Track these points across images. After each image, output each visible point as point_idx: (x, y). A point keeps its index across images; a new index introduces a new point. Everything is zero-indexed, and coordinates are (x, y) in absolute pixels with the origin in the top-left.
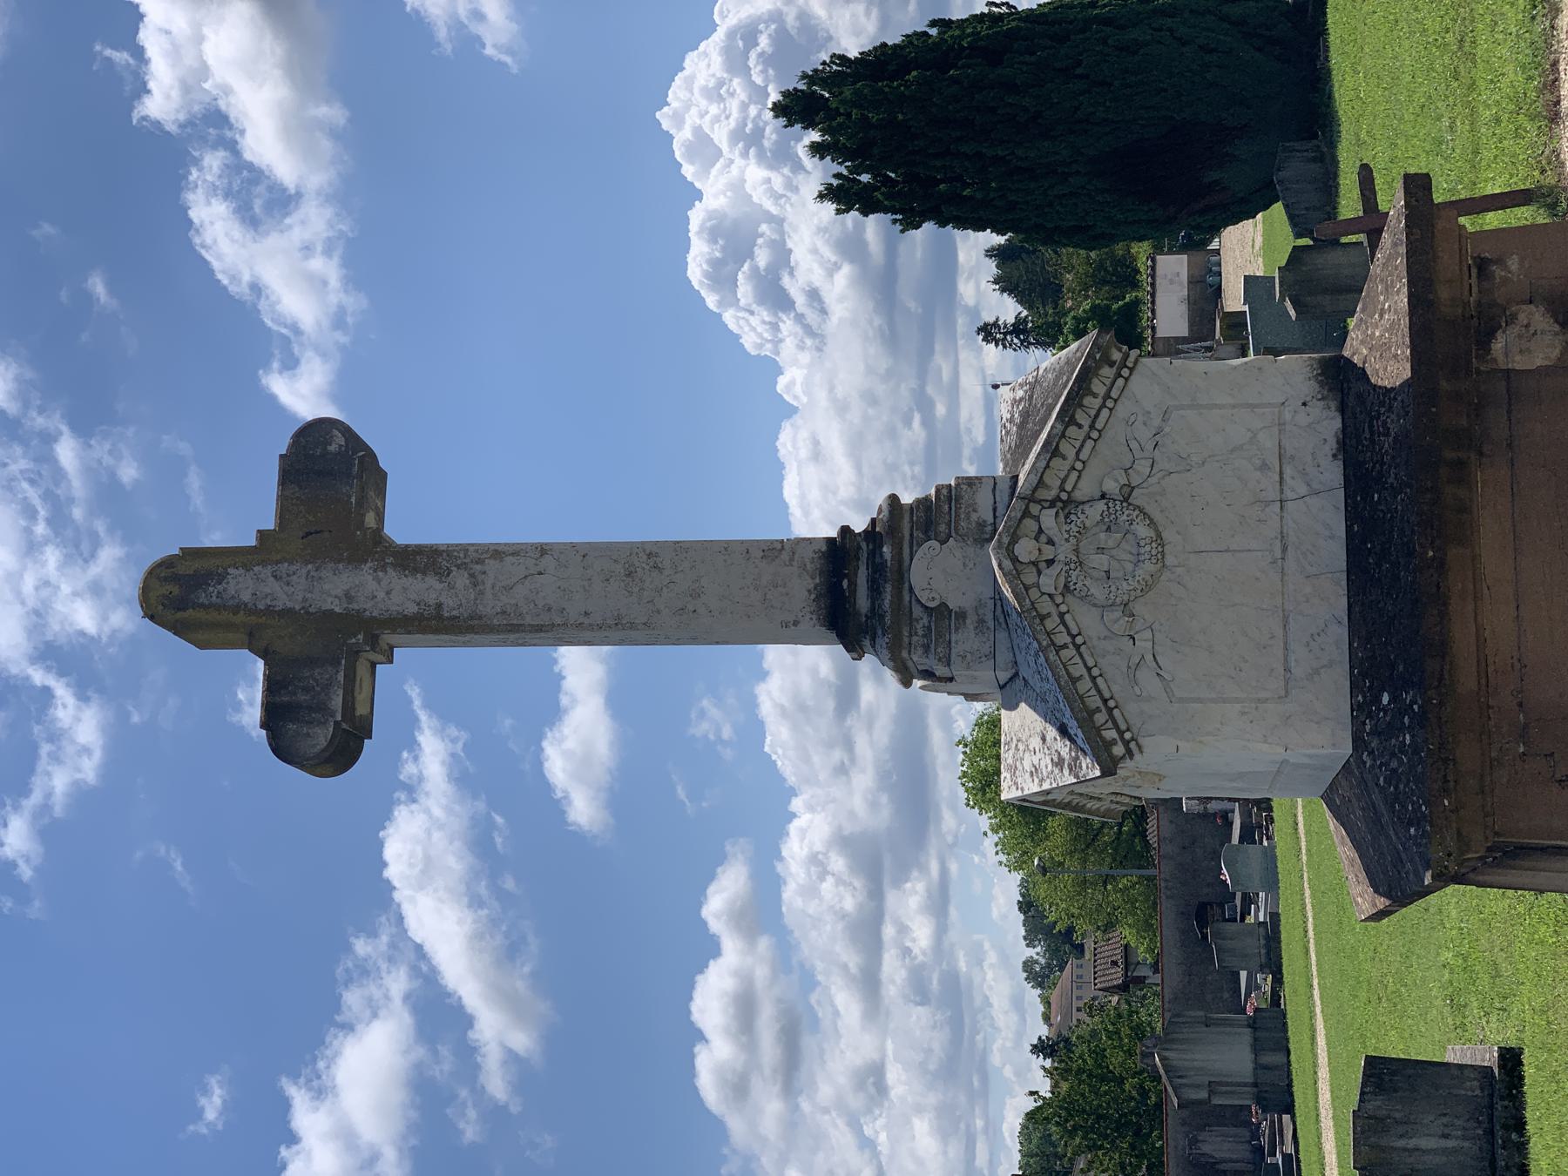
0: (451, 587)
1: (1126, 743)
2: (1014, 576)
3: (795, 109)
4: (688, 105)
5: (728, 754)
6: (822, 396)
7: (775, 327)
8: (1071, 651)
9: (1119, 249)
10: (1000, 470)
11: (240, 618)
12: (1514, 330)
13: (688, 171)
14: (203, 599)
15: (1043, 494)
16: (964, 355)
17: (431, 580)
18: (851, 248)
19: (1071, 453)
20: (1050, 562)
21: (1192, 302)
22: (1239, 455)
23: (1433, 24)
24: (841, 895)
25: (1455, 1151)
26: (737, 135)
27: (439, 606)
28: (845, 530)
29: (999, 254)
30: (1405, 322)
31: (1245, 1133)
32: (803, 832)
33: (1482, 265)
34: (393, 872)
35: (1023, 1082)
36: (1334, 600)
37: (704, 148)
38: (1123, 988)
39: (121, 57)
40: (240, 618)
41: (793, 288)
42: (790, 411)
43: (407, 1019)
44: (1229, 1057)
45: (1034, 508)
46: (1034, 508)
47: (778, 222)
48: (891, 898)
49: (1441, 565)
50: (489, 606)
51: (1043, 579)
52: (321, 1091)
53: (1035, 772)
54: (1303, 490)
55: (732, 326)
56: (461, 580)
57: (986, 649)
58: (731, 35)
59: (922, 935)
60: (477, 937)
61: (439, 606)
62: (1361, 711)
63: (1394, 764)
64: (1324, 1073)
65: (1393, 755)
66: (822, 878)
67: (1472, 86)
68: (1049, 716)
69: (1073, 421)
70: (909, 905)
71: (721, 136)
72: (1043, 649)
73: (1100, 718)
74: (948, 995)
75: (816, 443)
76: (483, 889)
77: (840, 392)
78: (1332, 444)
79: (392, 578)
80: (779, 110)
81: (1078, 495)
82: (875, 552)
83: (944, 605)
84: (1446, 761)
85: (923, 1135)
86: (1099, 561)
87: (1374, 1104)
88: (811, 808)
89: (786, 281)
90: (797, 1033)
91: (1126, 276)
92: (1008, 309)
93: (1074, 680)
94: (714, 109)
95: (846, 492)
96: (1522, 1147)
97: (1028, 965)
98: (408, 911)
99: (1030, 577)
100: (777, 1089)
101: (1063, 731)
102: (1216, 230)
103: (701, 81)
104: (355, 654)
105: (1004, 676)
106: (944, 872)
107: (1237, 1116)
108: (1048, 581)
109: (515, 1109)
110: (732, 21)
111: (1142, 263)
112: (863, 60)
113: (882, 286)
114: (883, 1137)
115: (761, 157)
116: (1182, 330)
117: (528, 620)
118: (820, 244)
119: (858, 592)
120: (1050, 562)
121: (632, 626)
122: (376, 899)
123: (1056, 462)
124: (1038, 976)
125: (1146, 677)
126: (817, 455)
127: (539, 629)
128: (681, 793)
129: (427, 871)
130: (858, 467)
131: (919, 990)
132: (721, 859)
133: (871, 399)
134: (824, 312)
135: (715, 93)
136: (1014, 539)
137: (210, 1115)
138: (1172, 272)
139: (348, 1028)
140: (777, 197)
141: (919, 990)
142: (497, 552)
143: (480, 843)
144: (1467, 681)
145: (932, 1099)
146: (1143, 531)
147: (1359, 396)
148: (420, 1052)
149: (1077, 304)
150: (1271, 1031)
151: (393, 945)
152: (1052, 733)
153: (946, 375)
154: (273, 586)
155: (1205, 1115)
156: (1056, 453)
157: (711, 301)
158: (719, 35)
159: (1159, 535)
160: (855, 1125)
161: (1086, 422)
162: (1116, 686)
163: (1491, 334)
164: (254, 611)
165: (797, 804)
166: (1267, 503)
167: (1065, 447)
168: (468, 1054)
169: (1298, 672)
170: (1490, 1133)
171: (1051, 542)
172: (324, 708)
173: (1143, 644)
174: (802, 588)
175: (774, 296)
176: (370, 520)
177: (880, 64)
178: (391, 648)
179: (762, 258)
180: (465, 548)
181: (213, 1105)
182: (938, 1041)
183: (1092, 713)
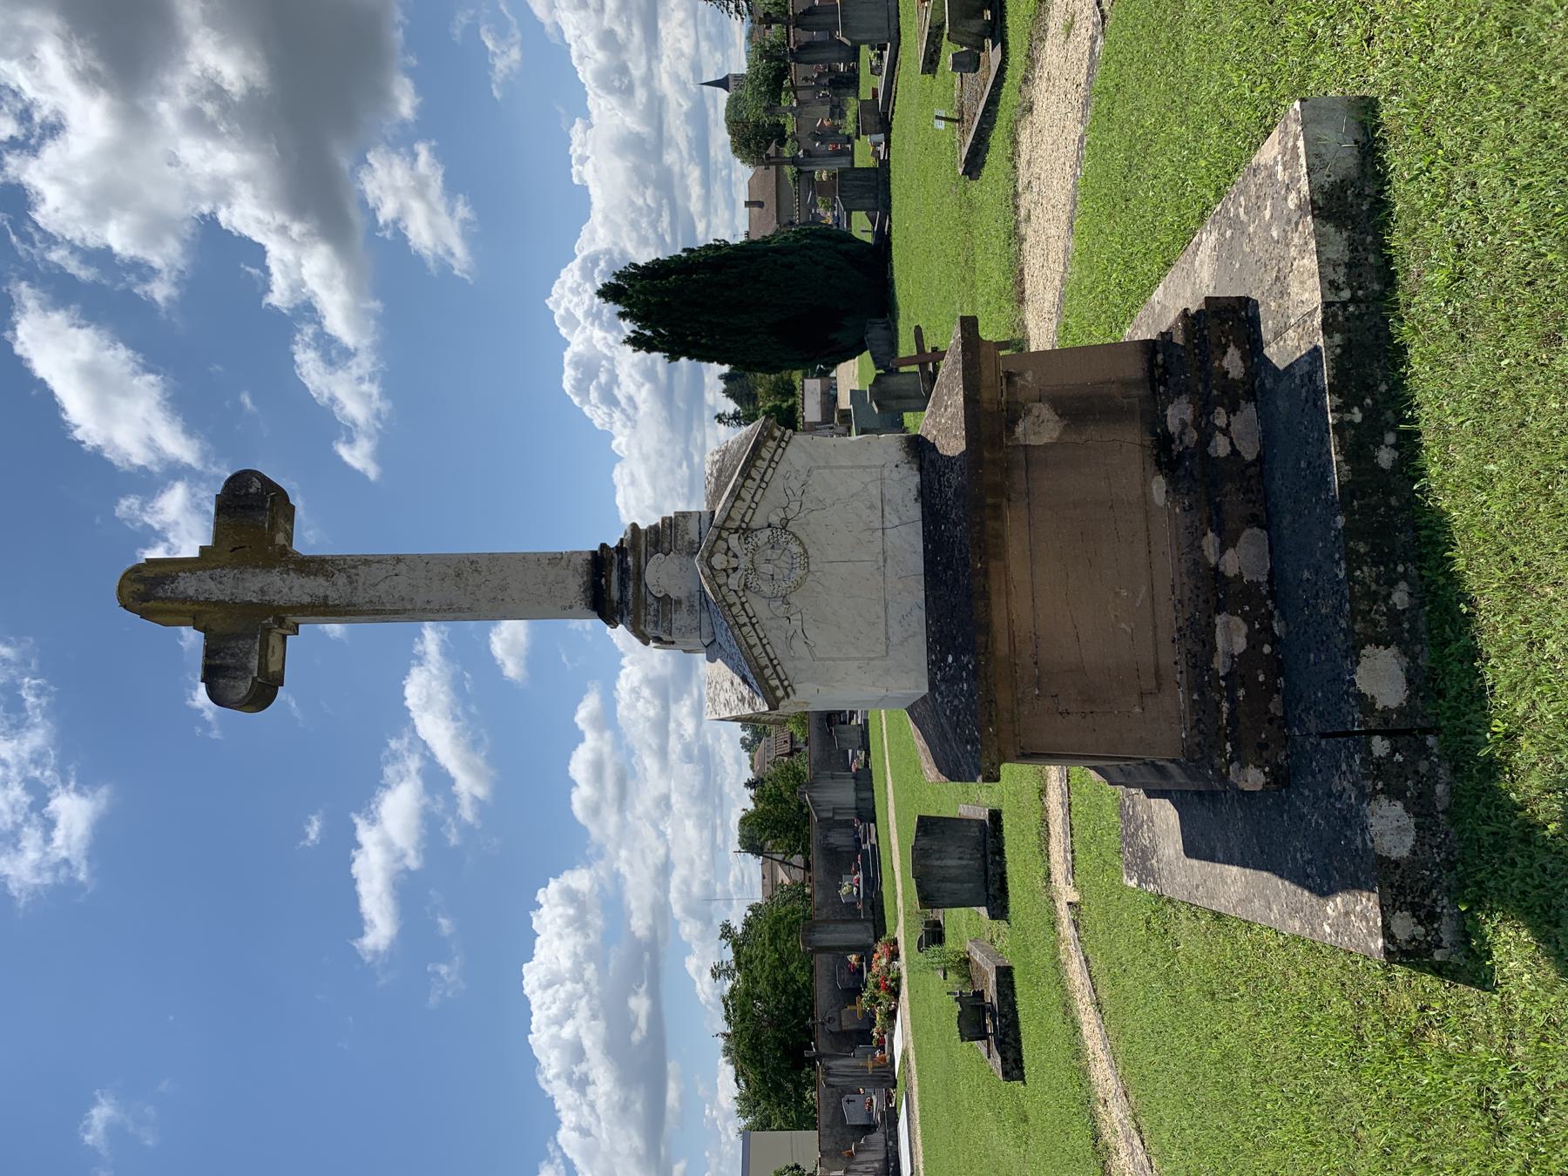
0: (334, 584)
1: (785, 688)
2: (712, 578)
3: (609, 293)
4: (563, 297)
5: (589, 638)
6: (635, 451)
7: (610, 416)
8: (749, 628)
9: (785, 374)
10: (704, 507)
11: (188, 606)
12: (1031, 419)
13: (563, 331)
14: (161, 594)
15: (730, 524)
16: (708, 431)
17: (321, 580)
18: (649, 374)
19: (748, 497)
20: (735, 569)
21: (823, 404)
22: (857, 493)
23: (951, 252)
24: (647, 708)
25: (966, 866)
26: (588, 313)
27: (326, 597)
28: (603, 546)
29: (726, 378)
30: (961, 413)
31: (851, 831)
32: (628, 676)
33: (1009, 376)
34: (409, 703)
35: (742, 802)
36: (916, 593)
37: (570, 320)
38: (790, 754)
39: (255, 272)
40: (188, 606)
41: (620, 394)
42: (620, 459)
43: (419, 782)
44: (843, 795)
45: (725, 534)
46: (725, 534)
47: (611, 360)
48: (673, 709)
49: (985, 573)
50: (360, 598)
51: (730, 581)
52: (373, 821)
53: (727, 703)
54: (897, 522)
55: (588, 414)
56: (341, 580)
57: (695, 624)
58: (585, 260)
59: (689, 727)
60: (456, 737)
61: (326, 597)
62: (935, 665)
63: (956, 702)
64: (891, 804)
65: (956, 696)
66: (638, 700)
67: (973, 286)
68: (735, 669)
69: (749, 477)
70: (682, 711)
71: (579, 314)
72: (731, 628)
73: (768, 672)
74: (703, 758)
75: (632, 475)
76: (459, 712)
77: (645, 450)
78: (914, 492)
79: (295, 580)
80: (600, 294)
81: (753, 525)
82: (622, 561)
83: (667, 595)
84: (990, 702)
85: (690, 829)
86: (767, 569)
87: (924, 842)
88: (632, 664)
89: (616, 391)
90: (625, 781)
91: (789, 390)
92: (730, 407)
93: (751, 647)
94: (576, 300)
95: (649, 502)
96: (1002, 864)
97: (743, 740)
98: (417, 721)
99: (722, 580)
100: (615, 809)
101: (744, 680)
102: (834, 365)
103: (569, 284)
104: (269, 630)
105: (707, 642)
106: (700, 695)
107: (848, 824)
108: (734, 581)
109: (478, 827)
110: (586, 253)
111: (798, 383)
112: (646, 267)
113: (666, 395)
114: (669, 831)
115: (601, 326)
116: (818, 418)
117: (388, 607)
118: (633, 372)
119: (613, 584)
120: (735, 569)
121: (460, 610)
122: (401, 718)
123: (739, 503)
124: (747, 746)
125: (798, 644)
126: (633, 482)
127: (396, 612)
128: (564, 659)
129: (428, 702)
130: (654, 488)
131: (688, 756)
132: (586, 691)
133: (660, 454)
134: (636, 408)
135: (576, 291)
136: (711, 554)
137: (312, 836)
138: (812, 388)
139: (388, 787)
140: (610, 347)
141: (688, 756)
142: (366, 561)
143: (457, 686)
144: (1002, 648)
145: (694, 811)
146: (795, 548)
147: (932, 462)
148: (426, 800)
149: (765, 404)
150: (864, 780)
151: (410, 743)
152: (737, 680)
153: (699, 441)
154: (211, 585)
155: (829, 825)
156: (738, 497)
157: (576, 401)
158: (578, 261)
159: (806, 551)
160: (655, 825)
161: (758, 478)
162: (779, 651)
163: (1015, 422)
164: (197, 602)
165: (624, 661)
166: (874, 530)
167: (744, 493)
168: (452, 799)
169: (894, 640)
170: (985, 856)
171: (735, 556)
172: (245, 668)
173: (796, 623)
174: (575, 585)
175: (609, 399)
176: (280, 538)
177: (656, 270)
178: (297, 625)
179: (603, 378)
180: (344, 558)
181: (314, 830)
182: (697, 781)
183: (762, 669)
